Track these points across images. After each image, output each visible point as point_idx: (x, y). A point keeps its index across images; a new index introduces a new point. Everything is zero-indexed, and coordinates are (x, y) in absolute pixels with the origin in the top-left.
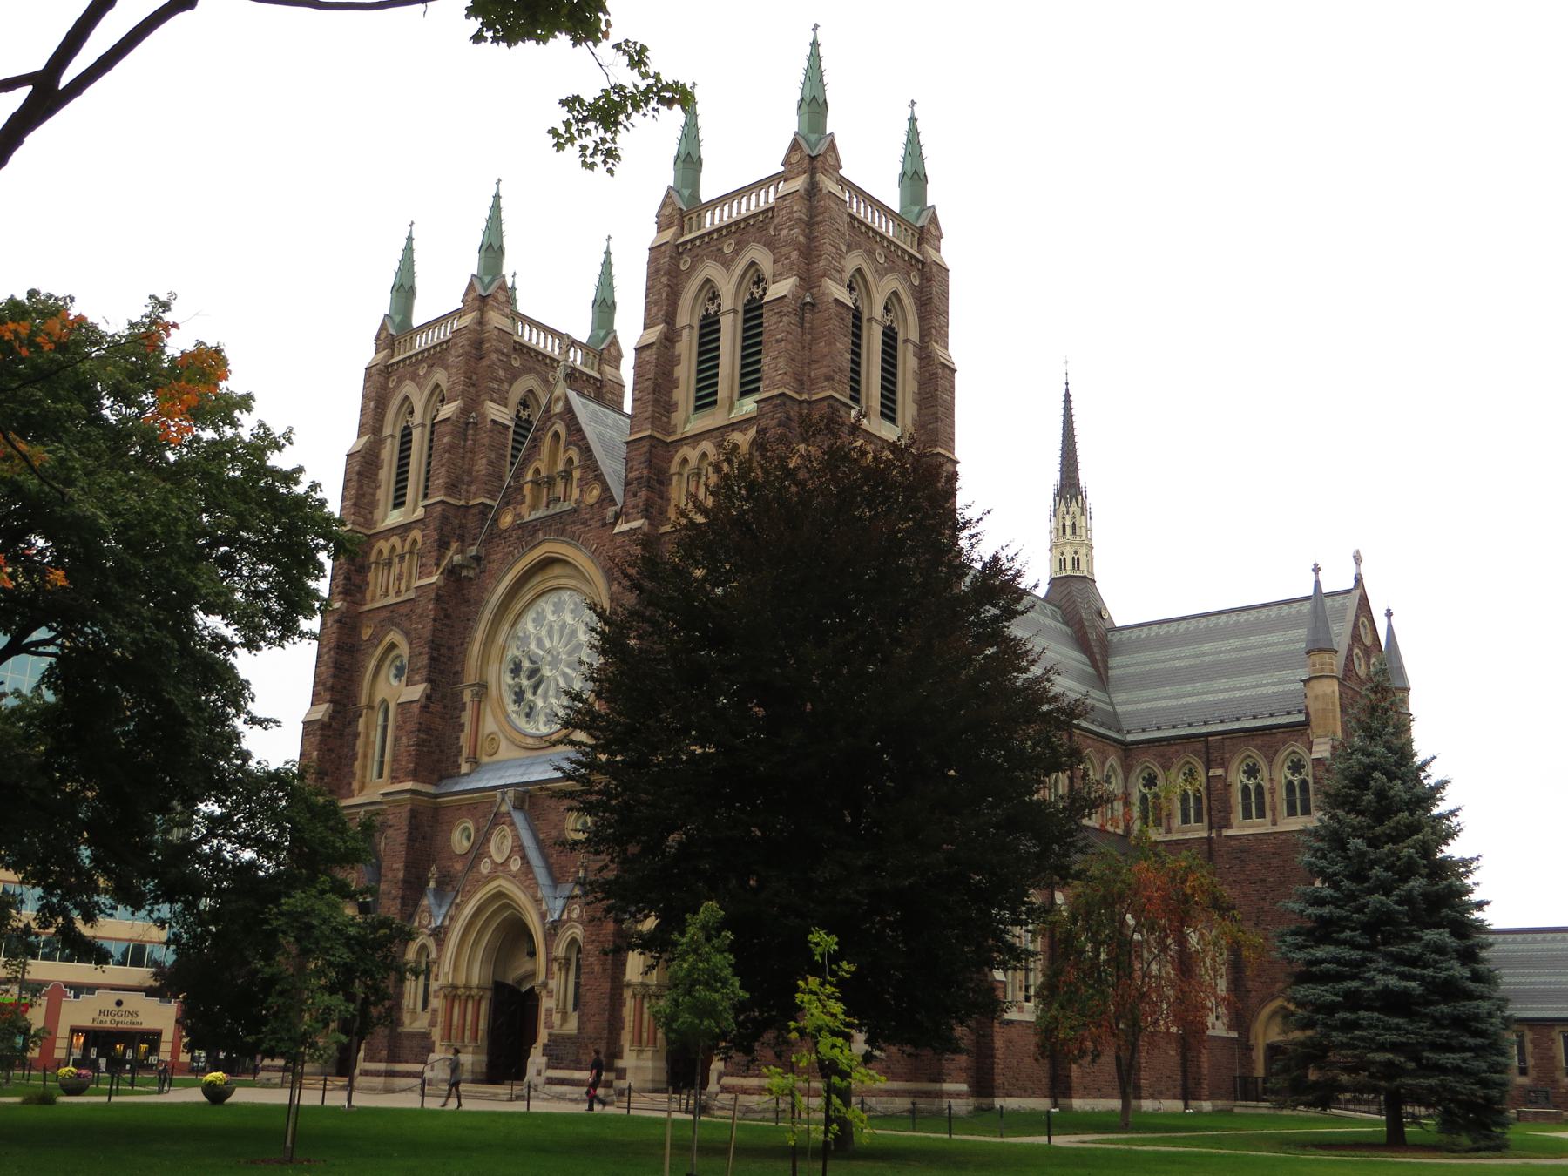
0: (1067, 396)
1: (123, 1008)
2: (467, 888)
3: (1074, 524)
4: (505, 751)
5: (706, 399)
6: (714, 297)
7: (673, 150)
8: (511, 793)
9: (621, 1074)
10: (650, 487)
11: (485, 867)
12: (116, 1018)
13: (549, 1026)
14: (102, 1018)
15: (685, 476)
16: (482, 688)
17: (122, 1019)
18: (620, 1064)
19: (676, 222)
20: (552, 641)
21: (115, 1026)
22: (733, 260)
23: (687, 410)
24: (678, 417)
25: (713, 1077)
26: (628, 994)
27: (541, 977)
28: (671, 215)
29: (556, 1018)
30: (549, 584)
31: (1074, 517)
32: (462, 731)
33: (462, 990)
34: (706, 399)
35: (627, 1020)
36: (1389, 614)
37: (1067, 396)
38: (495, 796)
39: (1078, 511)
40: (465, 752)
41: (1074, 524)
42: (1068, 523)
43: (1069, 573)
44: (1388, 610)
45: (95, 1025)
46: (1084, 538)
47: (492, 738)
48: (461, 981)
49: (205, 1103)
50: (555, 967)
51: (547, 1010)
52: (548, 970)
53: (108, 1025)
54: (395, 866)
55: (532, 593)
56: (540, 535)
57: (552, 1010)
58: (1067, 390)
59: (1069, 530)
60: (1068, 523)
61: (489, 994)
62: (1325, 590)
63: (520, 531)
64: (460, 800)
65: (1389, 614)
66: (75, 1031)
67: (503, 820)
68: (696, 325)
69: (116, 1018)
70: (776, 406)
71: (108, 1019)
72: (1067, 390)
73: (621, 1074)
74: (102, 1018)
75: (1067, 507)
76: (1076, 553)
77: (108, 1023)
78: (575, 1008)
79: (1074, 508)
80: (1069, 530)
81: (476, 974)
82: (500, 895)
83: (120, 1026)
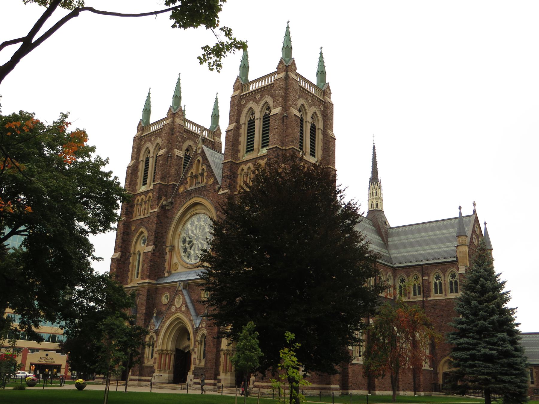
0: (374, 148)
1: (48, 357)
2: (167, 316)
3: (376, 192)
4: (180, 269)
5: (250, 148)
6: (253, 114)
7: (239, 64)
8: (182, 283)
9: (219, 381)
10: (231, 179)
11: (173, 309)
12: (46, 360)
13: (195, 364)
14: (41, 360)
15: (243, 175)
16: (173, 247)
17: (48, 360)
18: (219, 377)
19: (240, 88)
20: (196, 231)
21: (45, 363)
22: (259, 101)
23: (243, 153)
24: (240, 155)
25: (251, 382)
26: (222, 353)
27: (192, 347)
28: (238, 86)
29: (197, 361)
30: (196, 212)
31: (376, 190)
32: (166, 262)
33: (165, 351)
34: (250, 148)
35: (222, 362)
36: (485, 223)
37: (374, 148)
38: (177, 284)
39: (378, 188)
40: (166, 269)
41: (376, 192)
42: (374, 191)
43: (374, 209)
44: (485, 222)
45: (39, 362)
46: (380, 197)
47: (176, 265)
48: (165, 348)
49: (76, 390)
50: (197, 344)
51: (194, 359)
52: (195, 345)
53: (43, 362)
54: (142, 308)
55: (190, 215)
56: (193, 195)
57: (196, 359)
58: (374, 146)
59: (374, 194)
60: (374, 191)
61: (174, 353)
62: (463, 215)
63: (186, 193)
64: (164, 286)
65: (485, 223)
66: (32, 364)
67: (179, 293)
68: (247, 123)
69: (46, 360)
70: (274, 151)
71: (43, 360)
72: (374, 146)
73: (219, 381)
74: (41, 360)
75: (374, 186)
76: (377, 202)
77: (43, 362)
78: (204, 358)
79: (376, 186)
80: (374, 194)
81: (170, 346)
82: (178, 319)
83: (47, 363)
